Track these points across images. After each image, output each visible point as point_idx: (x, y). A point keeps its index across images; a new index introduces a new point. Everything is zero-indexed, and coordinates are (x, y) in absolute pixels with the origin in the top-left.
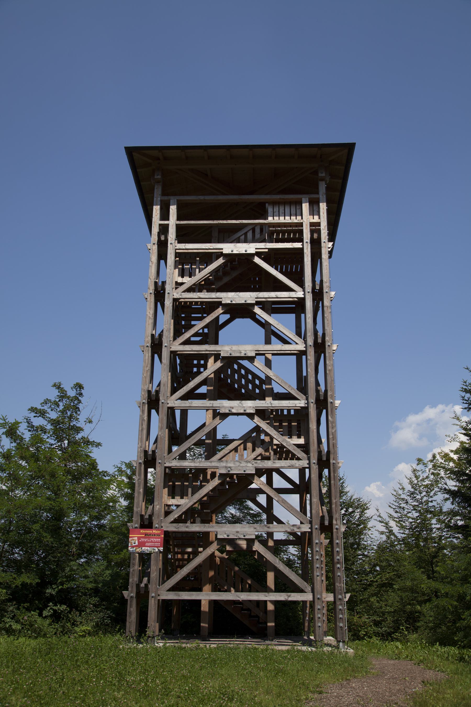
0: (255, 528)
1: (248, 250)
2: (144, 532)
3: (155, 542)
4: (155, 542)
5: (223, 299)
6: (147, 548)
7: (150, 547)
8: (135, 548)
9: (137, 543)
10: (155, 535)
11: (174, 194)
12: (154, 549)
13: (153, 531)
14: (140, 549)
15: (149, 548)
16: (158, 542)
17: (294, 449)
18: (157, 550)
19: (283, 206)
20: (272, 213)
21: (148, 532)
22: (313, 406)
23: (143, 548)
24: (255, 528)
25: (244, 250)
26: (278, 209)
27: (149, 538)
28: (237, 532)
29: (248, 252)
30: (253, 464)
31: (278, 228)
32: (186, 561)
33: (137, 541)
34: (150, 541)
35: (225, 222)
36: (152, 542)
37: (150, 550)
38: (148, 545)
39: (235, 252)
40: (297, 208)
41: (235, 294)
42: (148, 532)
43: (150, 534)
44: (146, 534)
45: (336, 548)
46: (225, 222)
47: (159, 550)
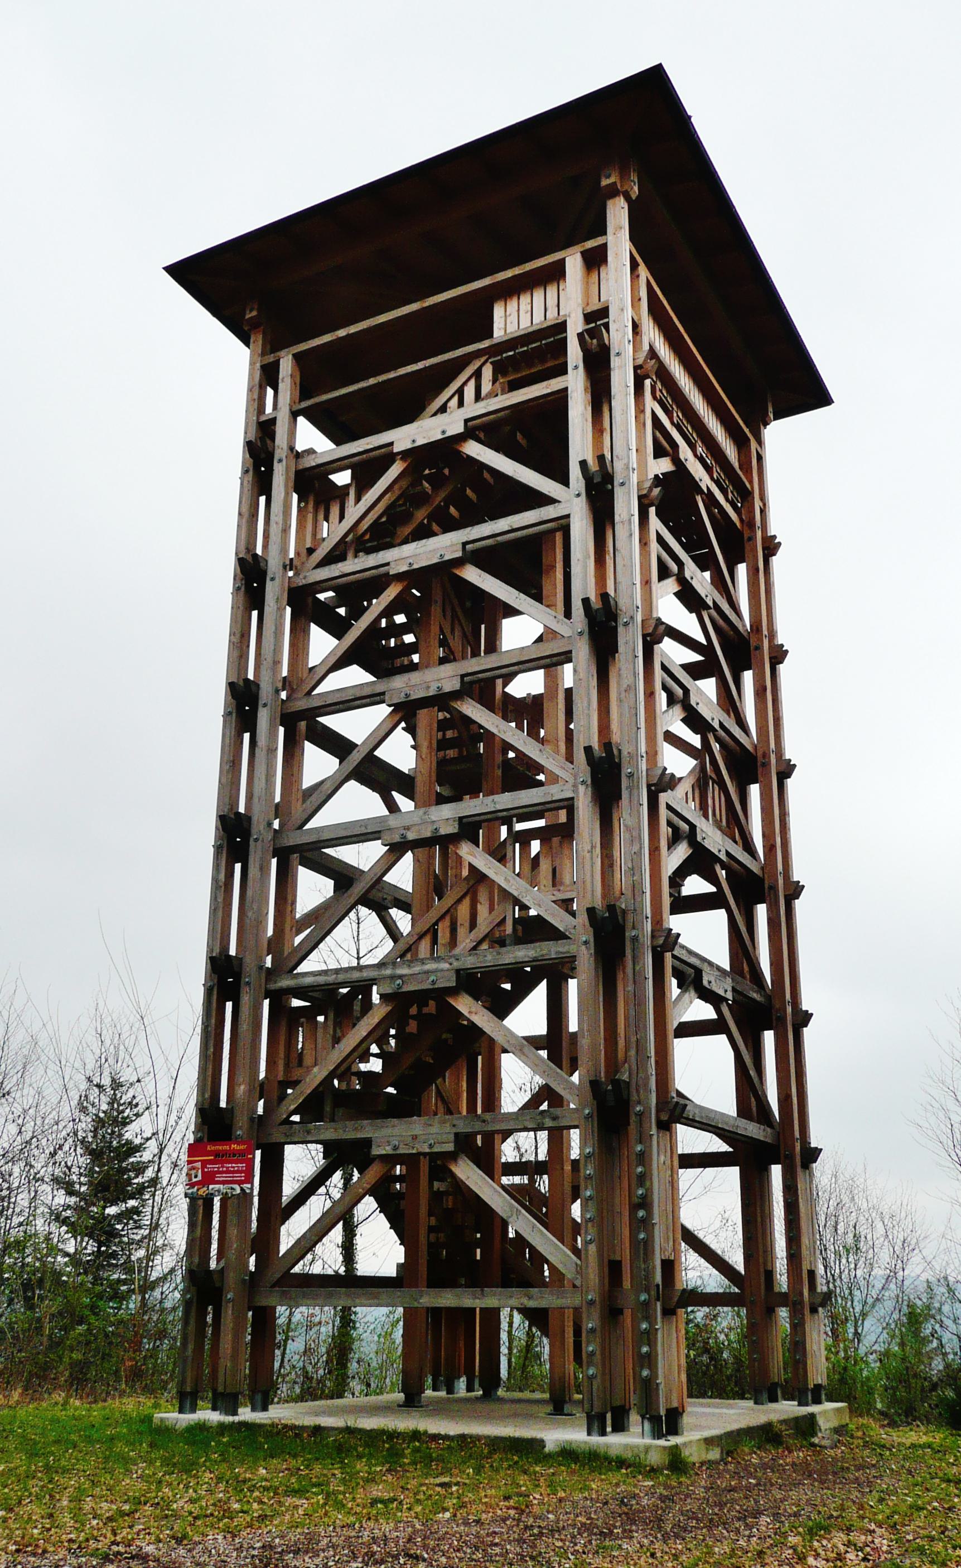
0: (454, 1126)
1: (416, 437)
2: (213, 1148)
3: (234, 1172)
4: (234, 1172)
5: (392, 565)
6: (217, 1186)
7: (223, 1183)
8: (196, 1188)
9: (199, 1178)
10: (234, 1155)
11: (568, 244)
12: (232, 1189)
13: (230, 1147)
14: (205, 1189)
15: (221, 1186)
16: (238, 1172)
17: (553, 915)
18: (238, 1191)
19: (503, 303)
20: (503, 319)
21: (220, 1148)
22: (585, 794)
23: (211, 1187)
24: (454, 1126)
25: (439, 431)
26: (556, 290)
27: (222, 1163)
28: (415, 1137)
29: (449, 434)
30: (451, 964)
31: (506, 352)
32: (576, 1241)
33: (200, 1171)
34: (225, 1169)
35: (392, 375)
36: (228, 1172)
37: (225, 1191)
38: (221, 1179)
39: (420, 442)
40: (561, 288)
41: (419, 546)
42: (220, 1148)
43: (224, 1153)
44: (216, 1154)
45: (637, 1166)
46: (392, 375)
47: (242, 1189)
